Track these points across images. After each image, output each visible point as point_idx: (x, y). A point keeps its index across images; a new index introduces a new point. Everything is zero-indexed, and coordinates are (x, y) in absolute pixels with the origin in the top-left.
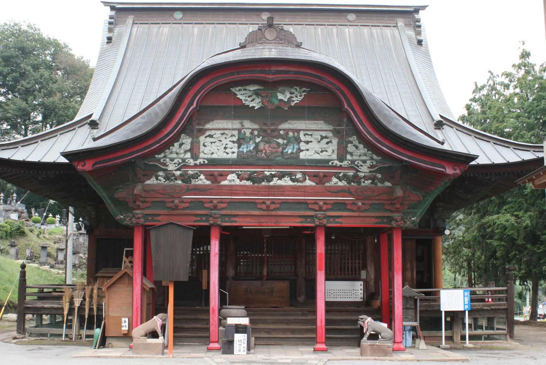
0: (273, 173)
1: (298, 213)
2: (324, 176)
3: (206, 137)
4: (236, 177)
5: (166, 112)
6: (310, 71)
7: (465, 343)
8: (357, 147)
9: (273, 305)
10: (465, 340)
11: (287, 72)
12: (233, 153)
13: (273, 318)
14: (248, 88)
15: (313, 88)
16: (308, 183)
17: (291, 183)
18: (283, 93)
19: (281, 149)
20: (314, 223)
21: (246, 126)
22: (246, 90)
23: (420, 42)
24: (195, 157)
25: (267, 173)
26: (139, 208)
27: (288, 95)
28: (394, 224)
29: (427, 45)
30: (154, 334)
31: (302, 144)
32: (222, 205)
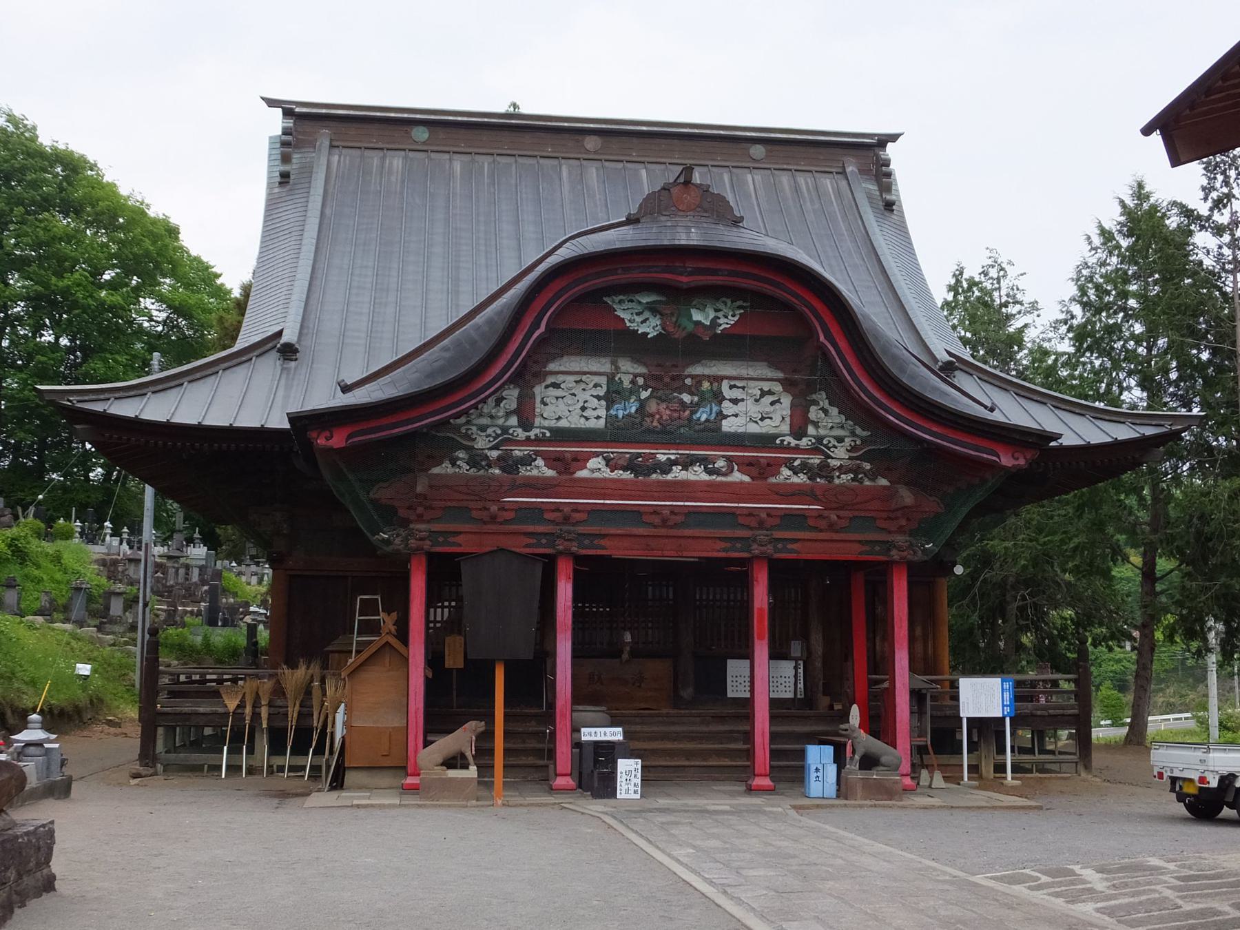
0: (673, 457)
1: (719, 533)
2: (769, 465)
3: (547, 387)
4: (603, 463)
5: (493, 341)
6: (756, 271)
7: (1005, 778)
8: (825, 412)
9: (643, 706)
10: (1005, 772)
11: (714, 272)
12: (598, 417)
13: (646, 729)
14: (638, 297)
15: (755, 301)
16: (737, 476)
17: (705, 477)
18: (702, 308)
19: (687, 412)
20: (554, 547)
21: (623, 369)
22: (632, 301)
23: (889, 206)
24: (526, 425)
25: (663, 458)
26: (420, 519)
27: (712, 314)
28: (895, 555)
29: (902, 212)
30: (454, 761)
31: (726, 404)
32: (577, 516)
